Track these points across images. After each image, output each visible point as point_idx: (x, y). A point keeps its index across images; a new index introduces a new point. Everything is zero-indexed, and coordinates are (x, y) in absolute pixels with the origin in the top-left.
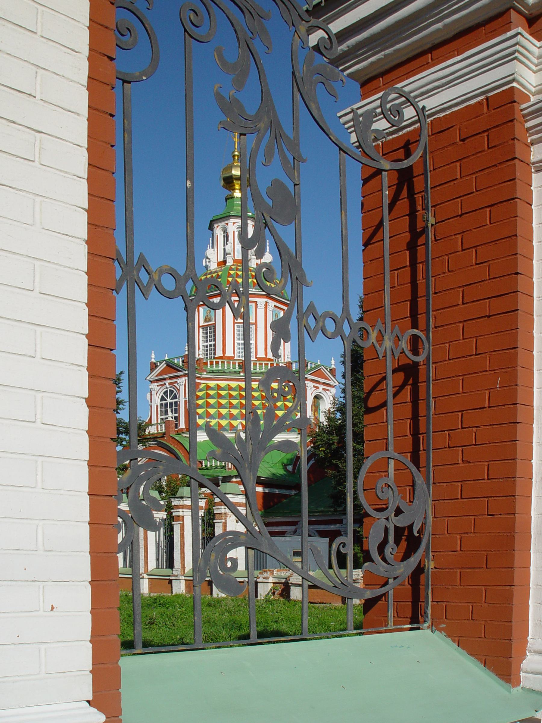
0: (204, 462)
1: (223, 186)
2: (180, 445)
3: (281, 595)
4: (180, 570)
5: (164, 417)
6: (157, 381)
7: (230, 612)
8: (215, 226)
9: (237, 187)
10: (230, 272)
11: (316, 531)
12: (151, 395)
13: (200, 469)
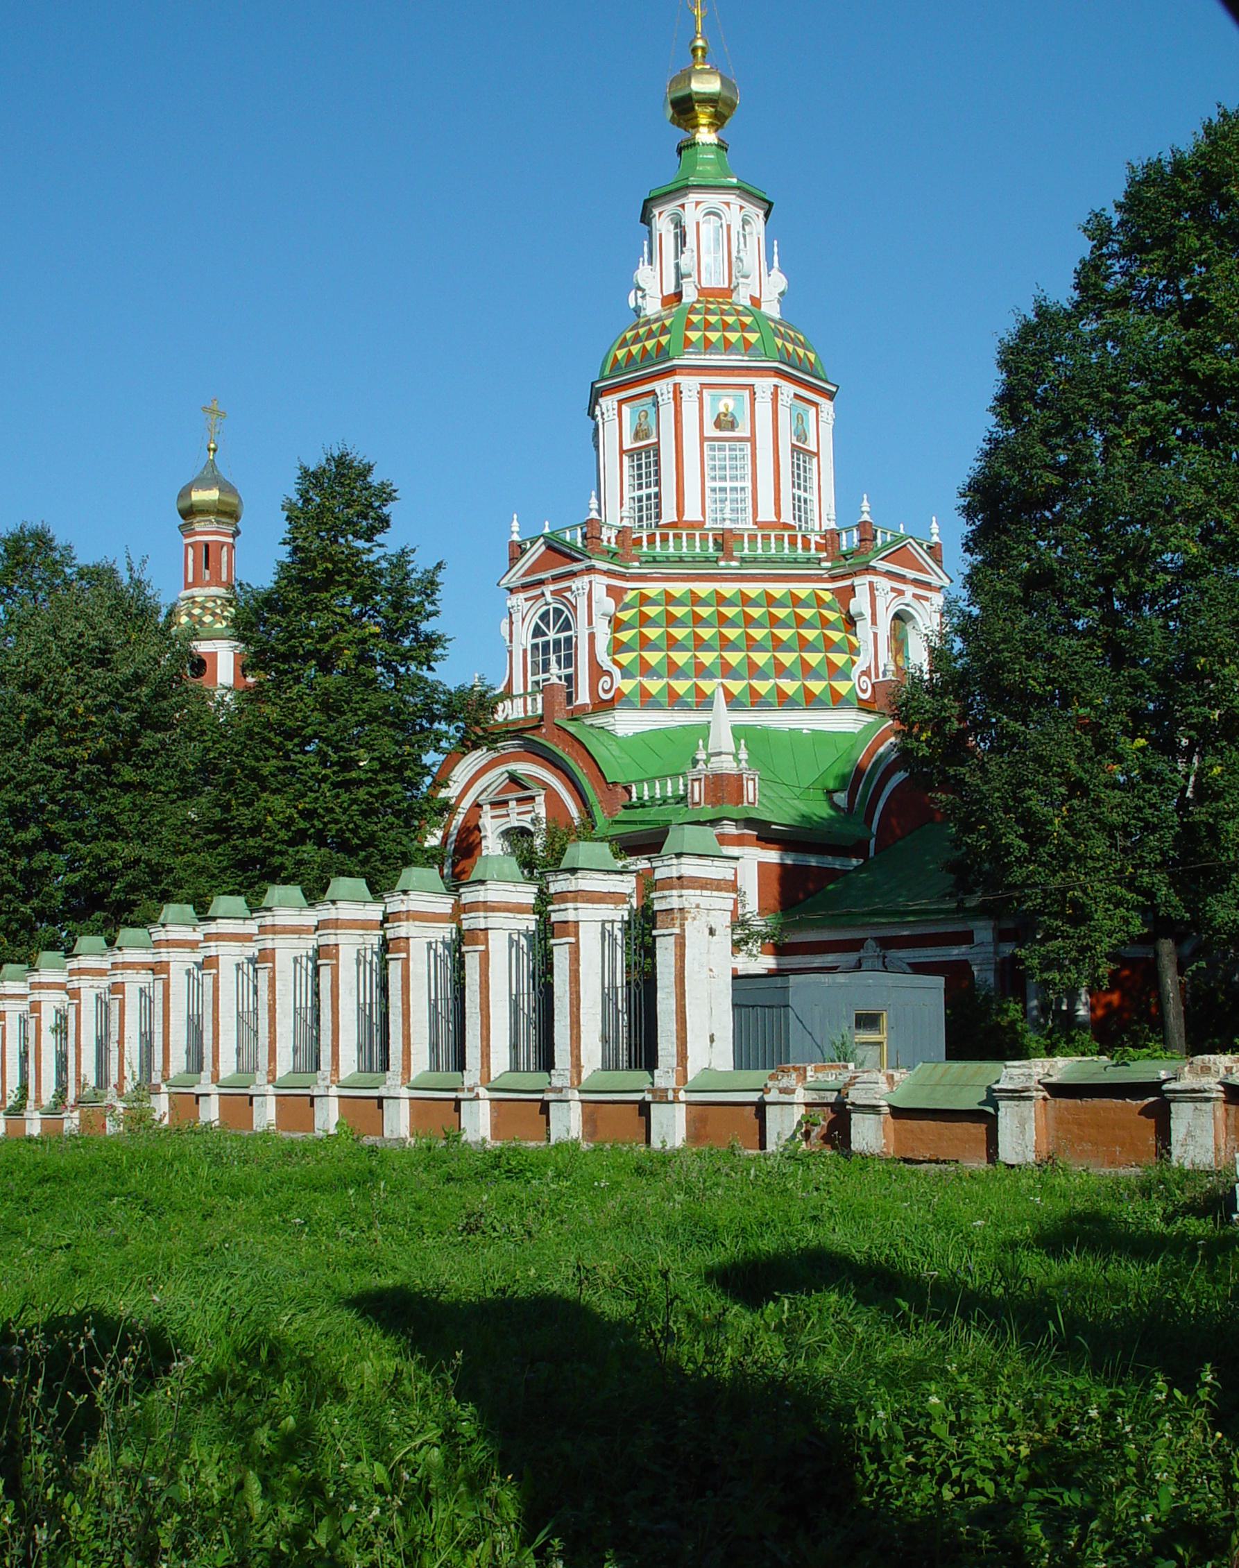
0: (634, 789)
1: (673, 120)
2: (577, 746)
3: (827, 1139)
4: (568, 1074)
5: (541, 676)
6: (526, 587)
7: (689, 1191)
8: (656, 212)
9: (703, 120)
10: (691, 317)
11: (909, 964)
12: (511, 623)
13: (625, 807)
